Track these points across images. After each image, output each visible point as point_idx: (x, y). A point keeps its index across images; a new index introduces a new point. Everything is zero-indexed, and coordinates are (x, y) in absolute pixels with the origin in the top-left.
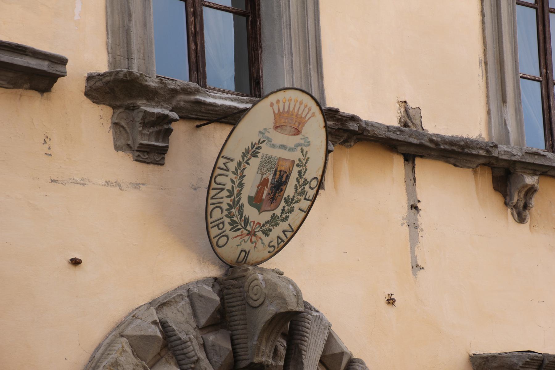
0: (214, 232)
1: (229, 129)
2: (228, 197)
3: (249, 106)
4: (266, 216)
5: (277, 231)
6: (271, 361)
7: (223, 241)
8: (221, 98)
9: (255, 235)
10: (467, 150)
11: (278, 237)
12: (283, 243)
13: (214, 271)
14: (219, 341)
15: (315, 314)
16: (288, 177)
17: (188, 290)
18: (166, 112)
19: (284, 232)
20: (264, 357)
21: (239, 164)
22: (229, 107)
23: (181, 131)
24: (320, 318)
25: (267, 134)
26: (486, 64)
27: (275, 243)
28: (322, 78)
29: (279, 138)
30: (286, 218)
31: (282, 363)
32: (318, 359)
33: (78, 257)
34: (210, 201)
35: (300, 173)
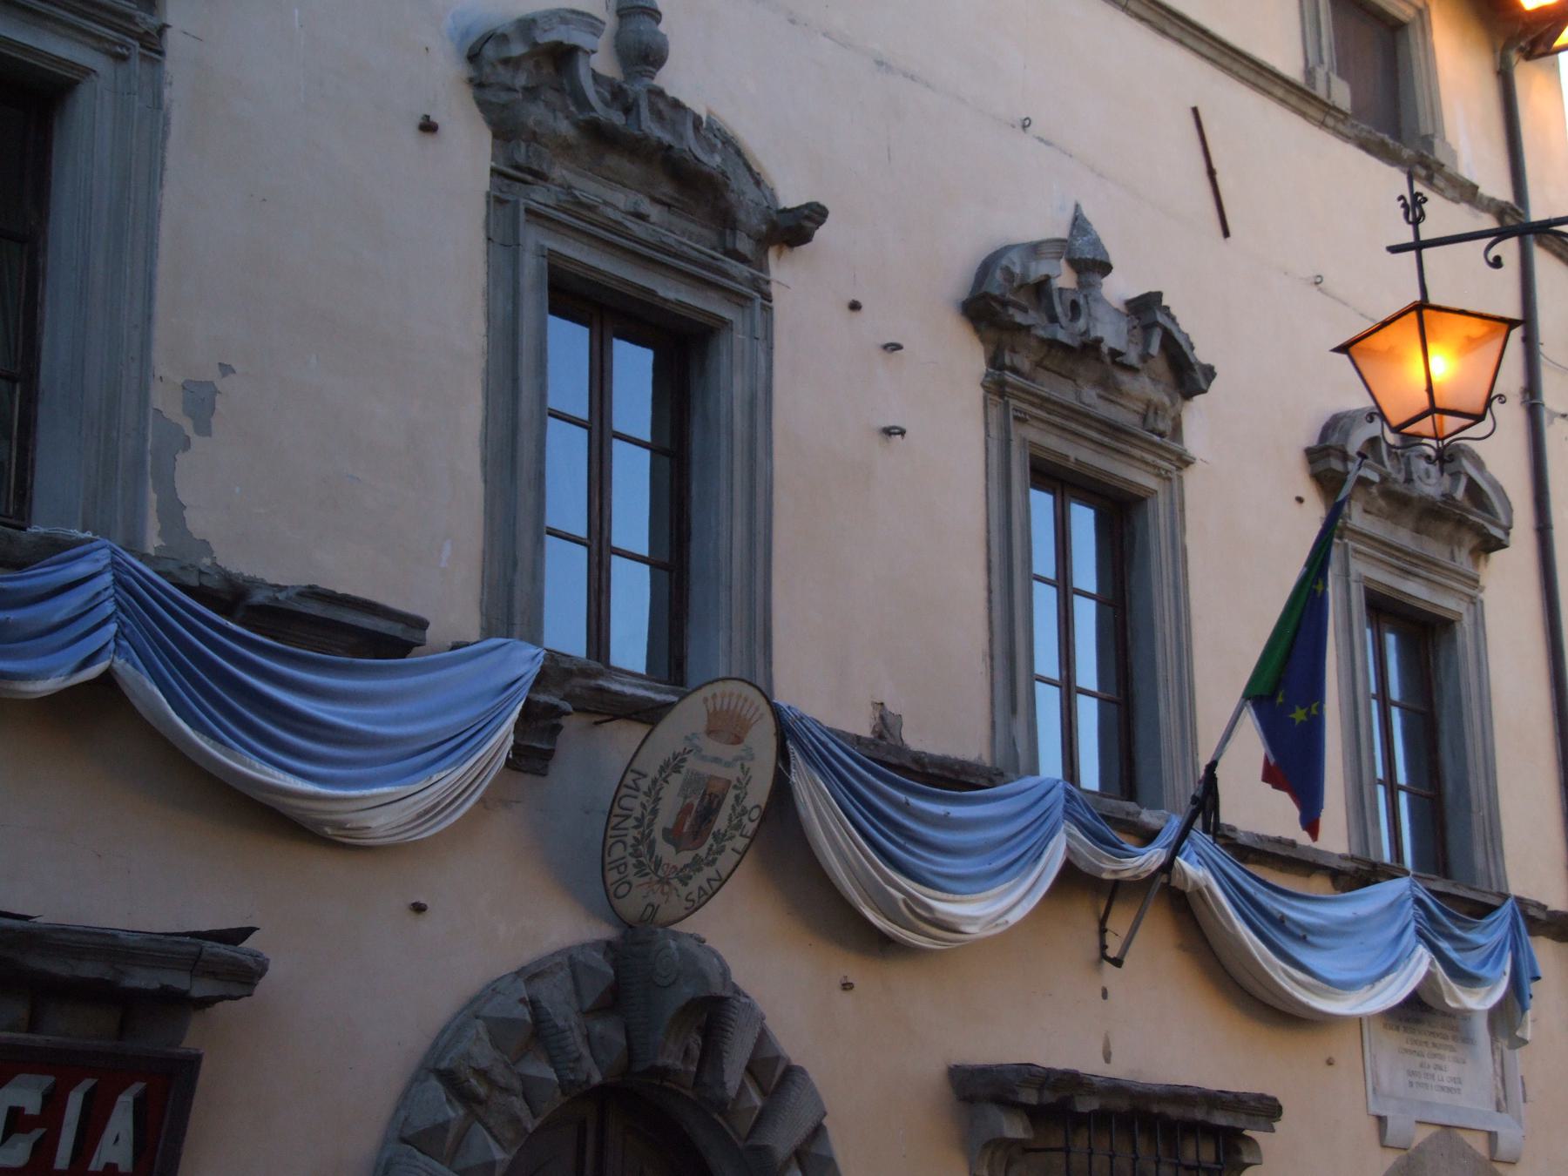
0: (613, 876)
1: (639, 731)
2: (636, 827)
3: (675, 699)
4: (687, 857)
5: (699, 880)
6: (679, 1065)
7: (623, 889)
8: (631, 685)
9: (668, 883)
10: (963, 778)
11: (701, 888)
12: (707, 896)
13: (604, 931)
14: (610, 1030)
15: (743, 1000)
16: (720, 804)
17: (570, 958)
18: (554, 700)
19: (709, 880)
20: (671, 1059)
21: (655, 781)
22: (642, 698)
23: (572, 725)
24: (750, 1007)
25: (696, 742)
26: (992, 658)
27: (695, 896)
28: (770, 663)
29: (712, 747)
30: (714, 861)
31: (693, 1068)
32: (745, 1063)
33: (422, 901)
34: (610, 832)
35: (737, 797)
